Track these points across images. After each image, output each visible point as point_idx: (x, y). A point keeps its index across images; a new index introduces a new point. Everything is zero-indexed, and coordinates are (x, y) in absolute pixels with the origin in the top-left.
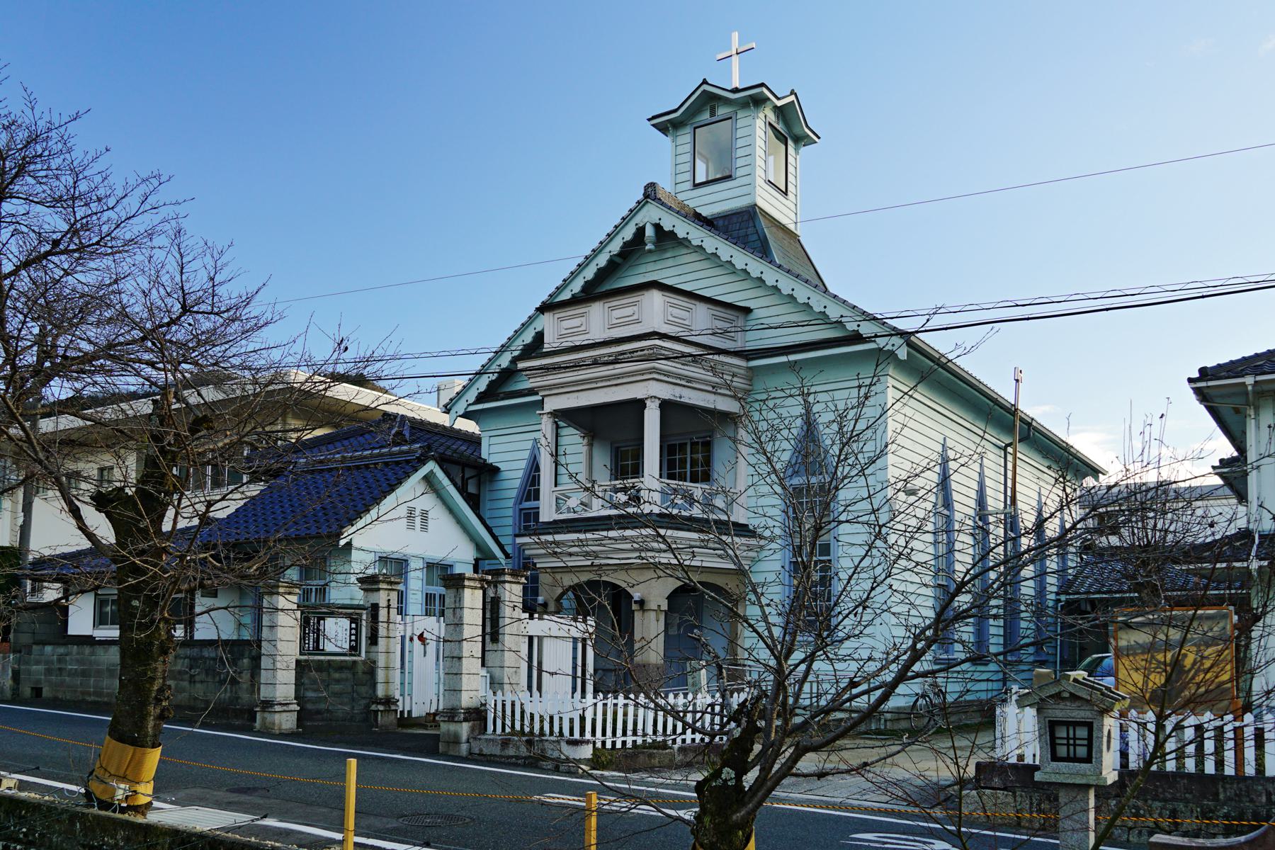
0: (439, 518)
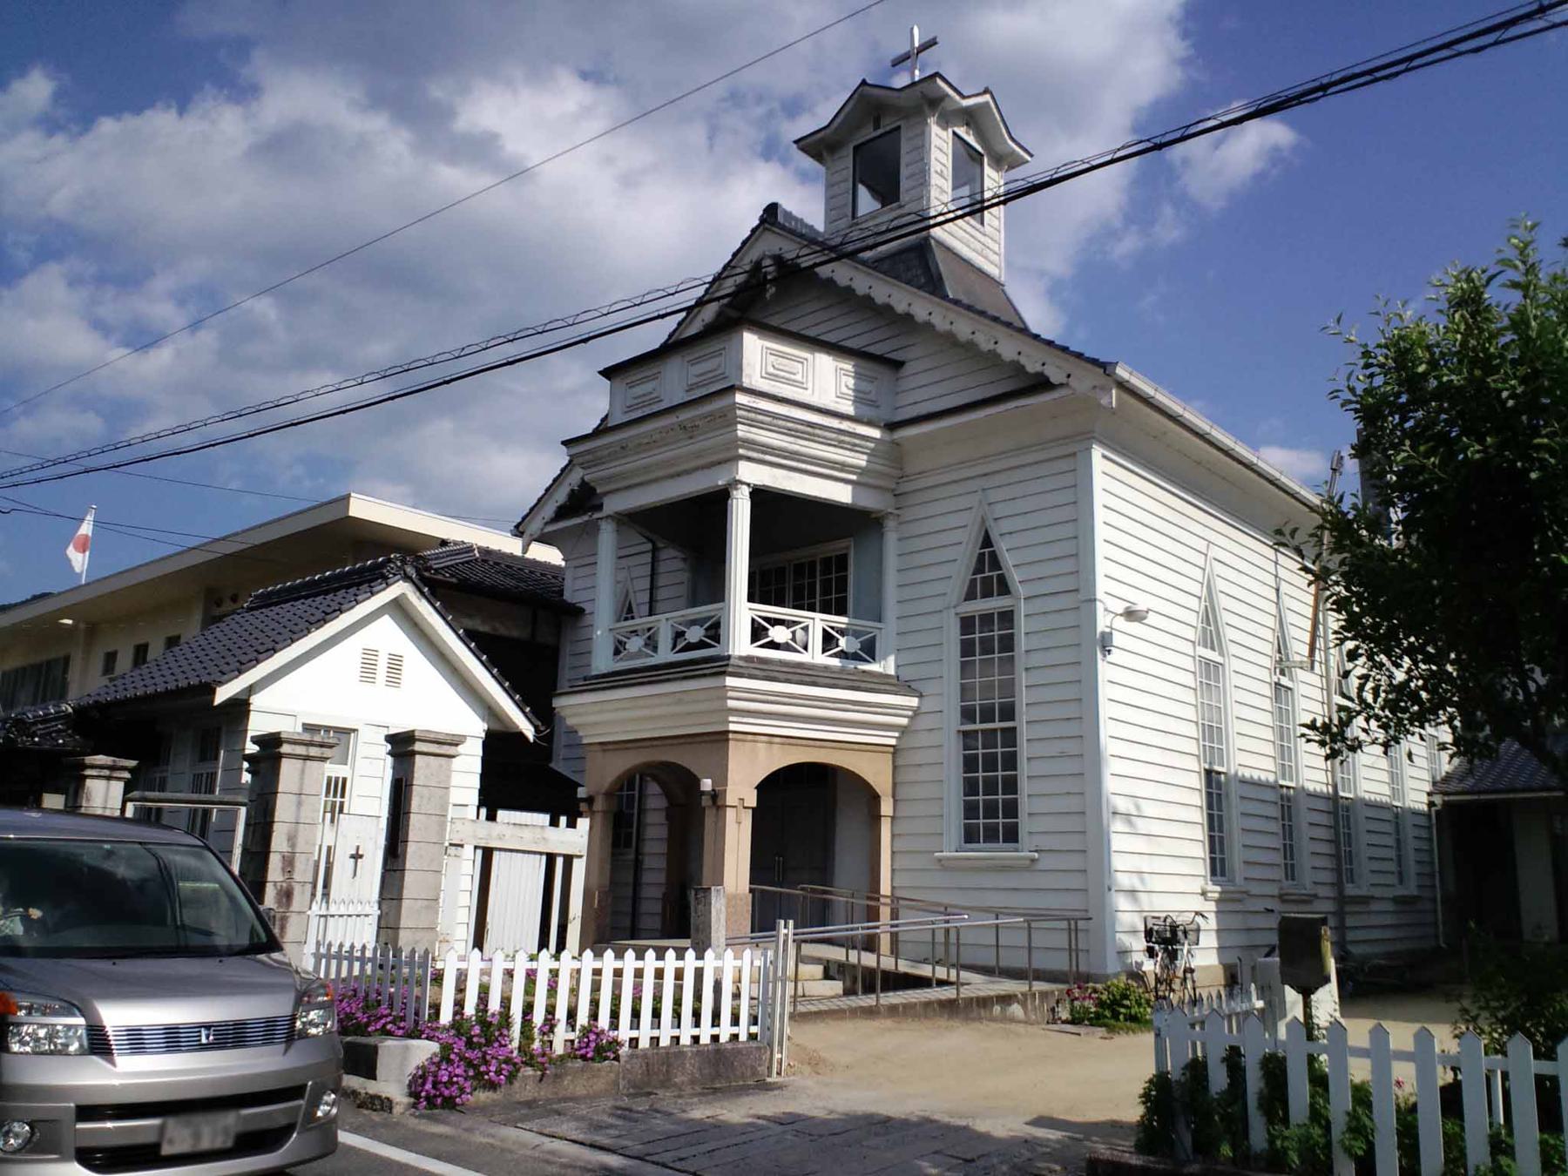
0: (416, 662)
